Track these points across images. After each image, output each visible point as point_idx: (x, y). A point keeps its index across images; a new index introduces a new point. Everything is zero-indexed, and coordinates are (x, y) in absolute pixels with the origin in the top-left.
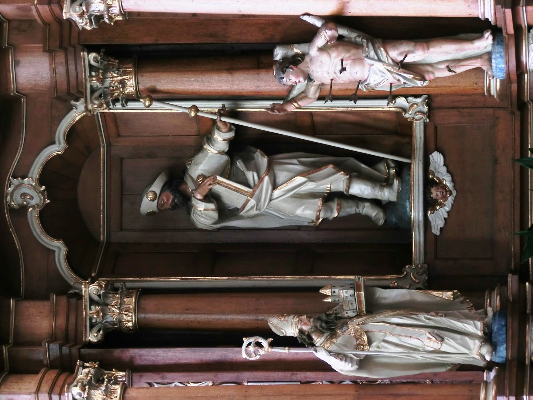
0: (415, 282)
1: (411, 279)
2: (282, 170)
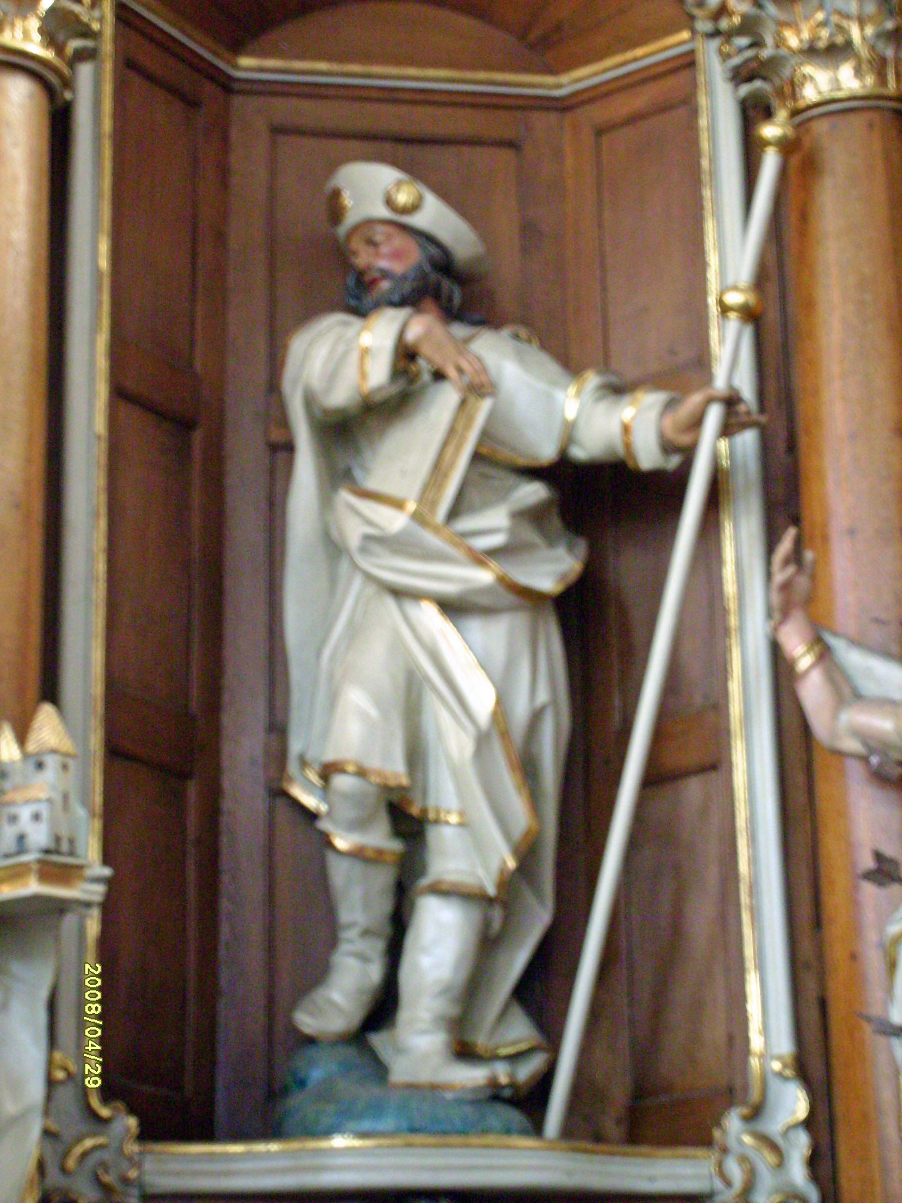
0: (66, 1154)
1: (79, 1140)
2: (511, 645)
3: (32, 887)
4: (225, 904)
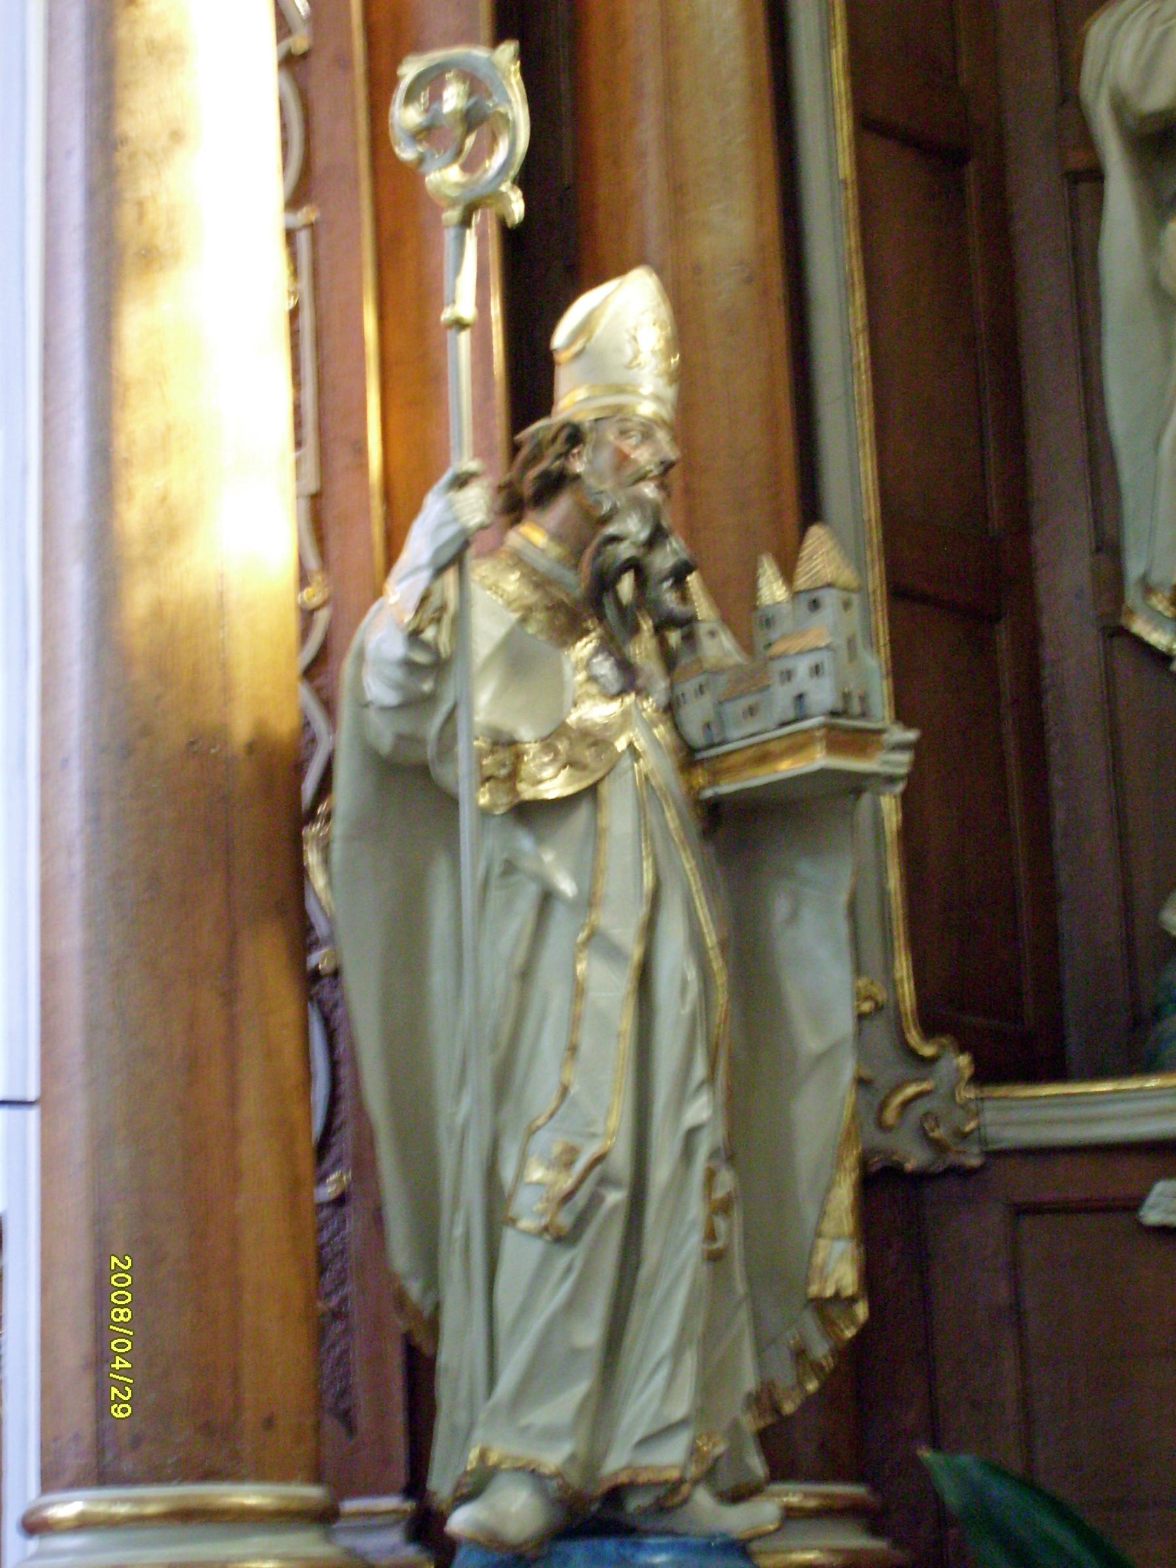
0: (883, 1106)
1: (899, 1087)
3: (818, 759)
4: (1057, 782)
